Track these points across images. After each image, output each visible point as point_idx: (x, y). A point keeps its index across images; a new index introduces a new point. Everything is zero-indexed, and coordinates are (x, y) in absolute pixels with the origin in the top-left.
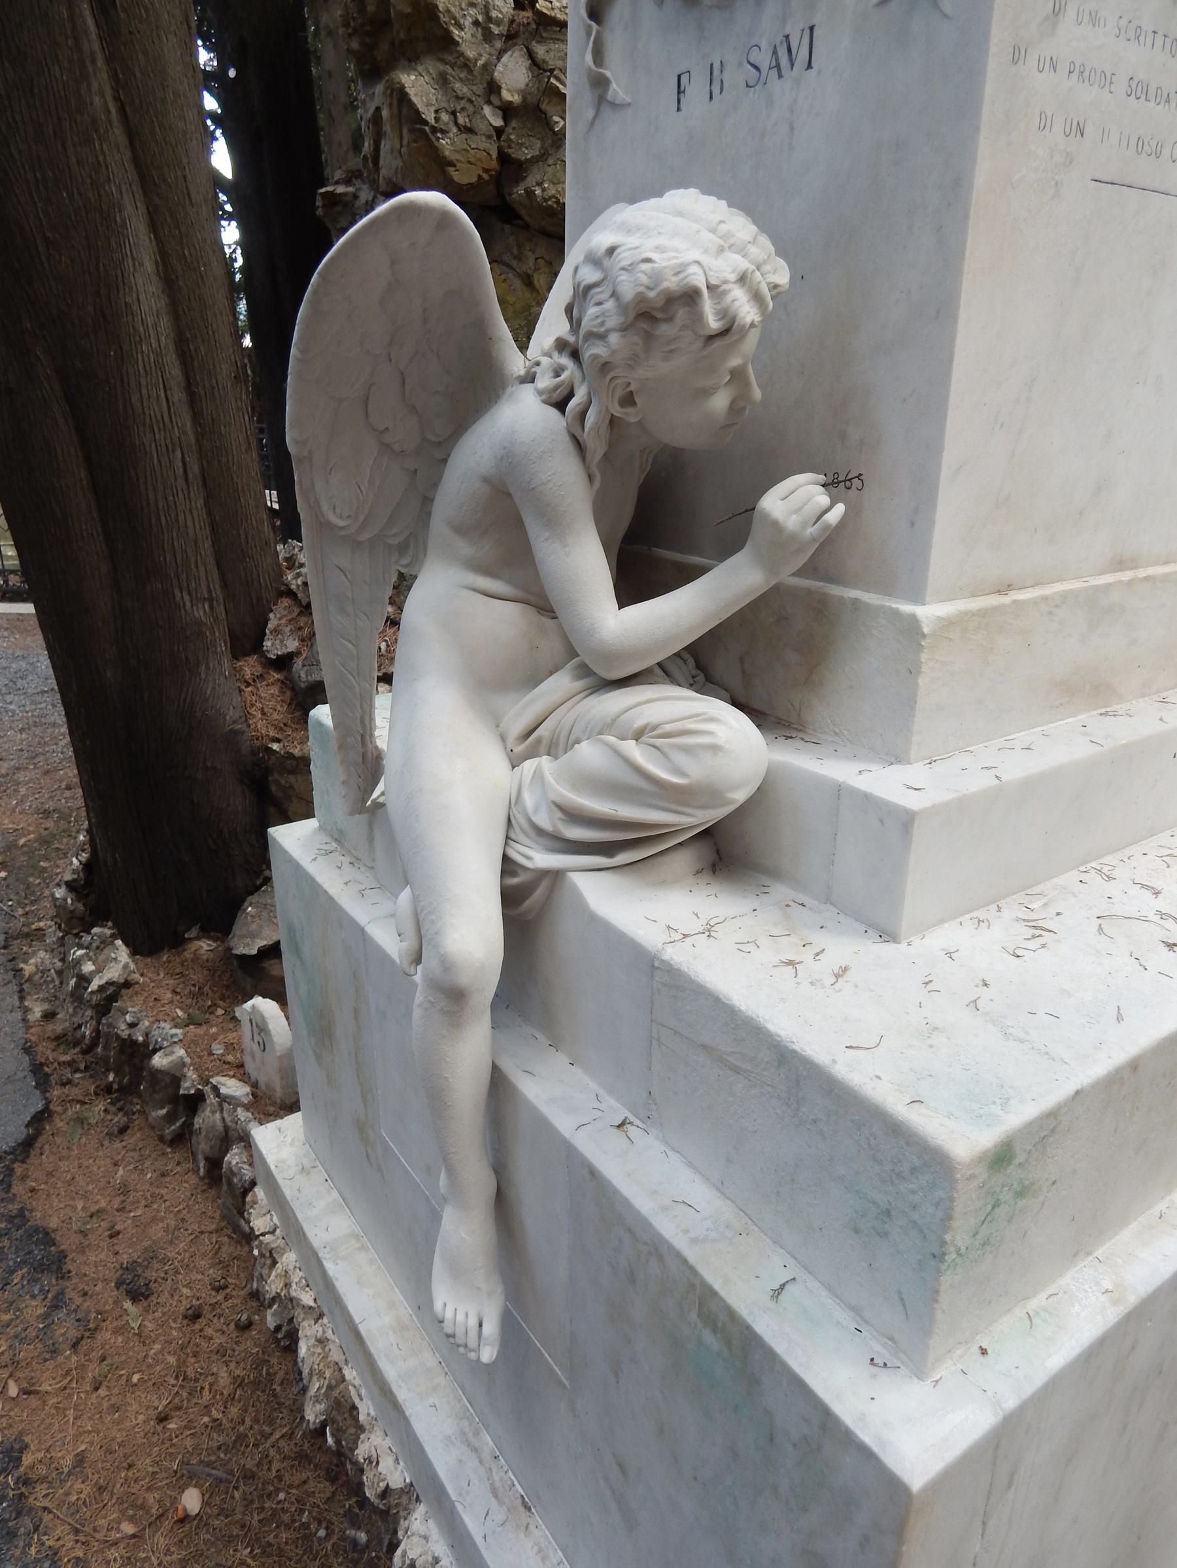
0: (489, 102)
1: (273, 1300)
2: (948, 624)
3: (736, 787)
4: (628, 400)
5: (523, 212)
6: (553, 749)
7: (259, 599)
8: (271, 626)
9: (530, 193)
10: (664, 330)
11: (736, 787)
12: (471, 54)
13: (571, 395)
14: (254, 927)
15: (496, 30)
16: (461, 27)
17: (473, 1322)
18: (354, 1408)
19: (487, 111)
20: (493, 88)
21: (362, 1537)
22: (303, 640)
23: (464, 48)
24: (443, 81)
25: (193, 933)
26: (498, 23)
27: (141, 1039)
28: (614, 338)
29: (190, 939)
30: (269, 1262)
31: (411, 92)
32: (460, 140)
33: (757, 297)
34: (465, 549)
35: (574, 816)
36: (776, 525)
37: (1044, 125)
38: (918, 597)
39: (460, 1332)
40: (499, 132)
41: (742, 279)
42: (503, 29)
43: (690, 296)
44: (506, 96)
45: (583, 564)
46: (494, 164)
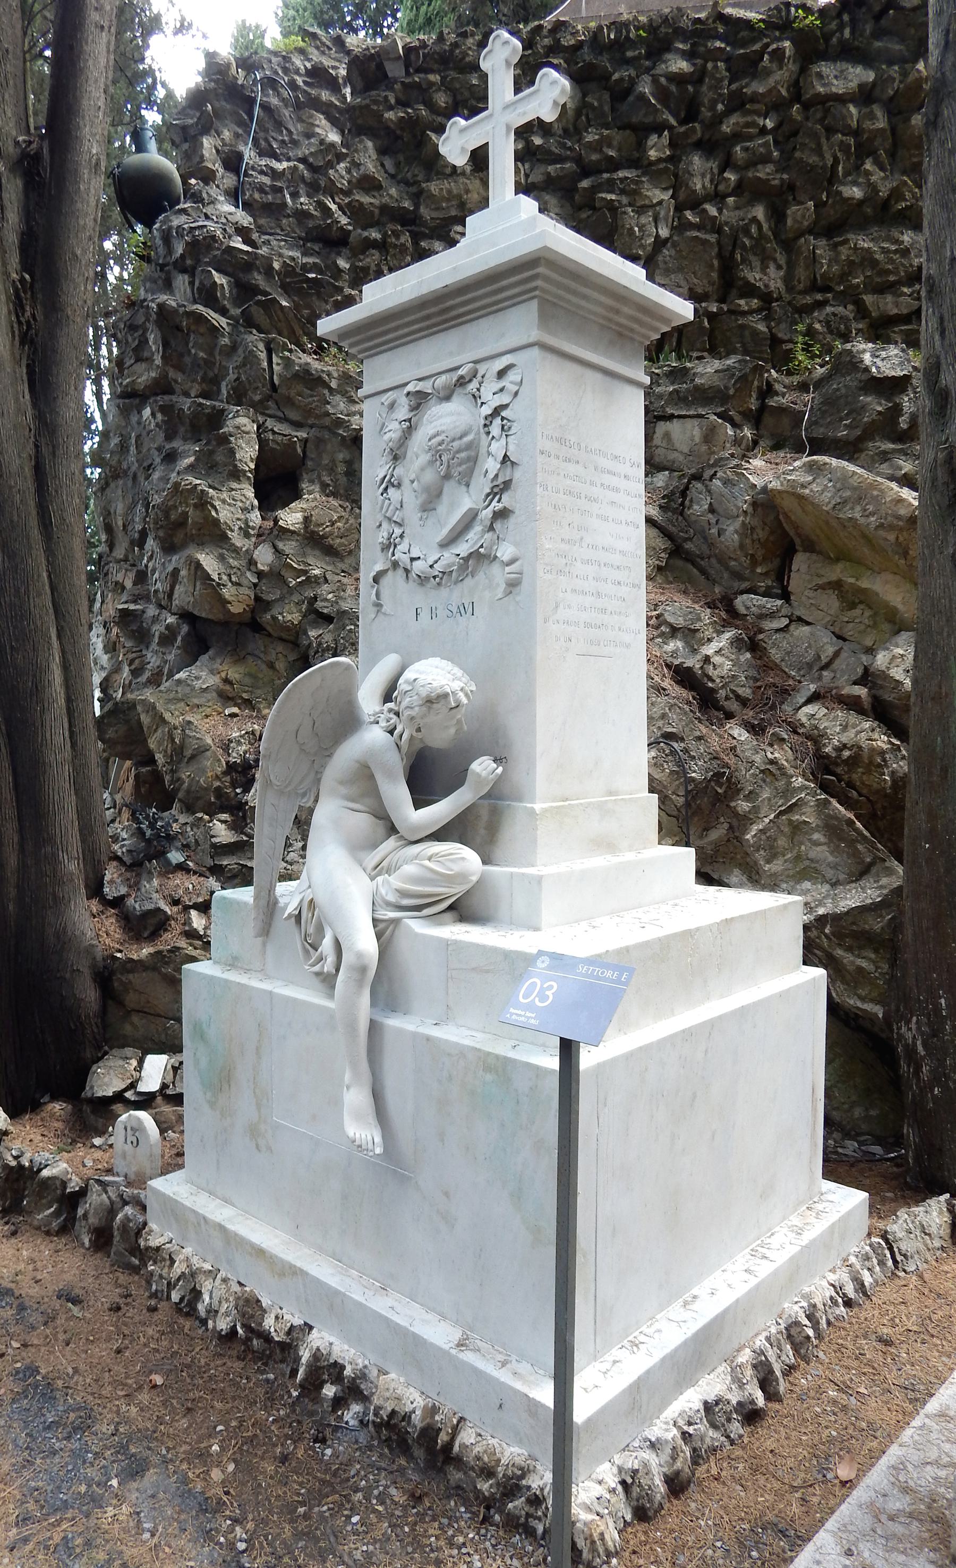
0: (249, 570)
1: (179, 1279)
2: (545, 811)
3: (472, 874)
4: (419, 730)
5: (269, 628)
6: (389, 871)
7: (99, 861)
8: (107, 878)
9: (274, 618)
10: (435, 706)
11: (472, 874)
12: (239, 544)
13: (395, 728)
14: (106, 1080)
15: (252, 532)
16: (232, 531)
17: (369, 1138)
18: (258, 1301)
19: (248, 574)
20: (252, 563)
21: (271, 1376)
22: (130, 887)
23: (233, 541)
24: (222, 558)
25: (46, 1099)
26: (253, 528)
27: (27, 1164)
28: (417, 709)
29: (45, 1103)
30: (168, 1263)
31: (204, 564)
32: (233, 590)
33: (466, 695)
34: (343, 790)
35: (403, 894)
36: (479, 775)
37: (558, 639)
38: (533, 801)
39: (364, 1142)
40: (255, 585)
41: (462, 690)
42: (256, 531)
43: (445, 696)
44: (260, 567)
45: (398, 794)
46: (252, 602)
